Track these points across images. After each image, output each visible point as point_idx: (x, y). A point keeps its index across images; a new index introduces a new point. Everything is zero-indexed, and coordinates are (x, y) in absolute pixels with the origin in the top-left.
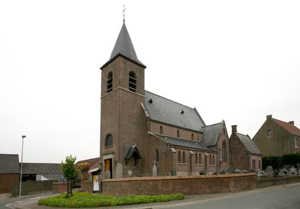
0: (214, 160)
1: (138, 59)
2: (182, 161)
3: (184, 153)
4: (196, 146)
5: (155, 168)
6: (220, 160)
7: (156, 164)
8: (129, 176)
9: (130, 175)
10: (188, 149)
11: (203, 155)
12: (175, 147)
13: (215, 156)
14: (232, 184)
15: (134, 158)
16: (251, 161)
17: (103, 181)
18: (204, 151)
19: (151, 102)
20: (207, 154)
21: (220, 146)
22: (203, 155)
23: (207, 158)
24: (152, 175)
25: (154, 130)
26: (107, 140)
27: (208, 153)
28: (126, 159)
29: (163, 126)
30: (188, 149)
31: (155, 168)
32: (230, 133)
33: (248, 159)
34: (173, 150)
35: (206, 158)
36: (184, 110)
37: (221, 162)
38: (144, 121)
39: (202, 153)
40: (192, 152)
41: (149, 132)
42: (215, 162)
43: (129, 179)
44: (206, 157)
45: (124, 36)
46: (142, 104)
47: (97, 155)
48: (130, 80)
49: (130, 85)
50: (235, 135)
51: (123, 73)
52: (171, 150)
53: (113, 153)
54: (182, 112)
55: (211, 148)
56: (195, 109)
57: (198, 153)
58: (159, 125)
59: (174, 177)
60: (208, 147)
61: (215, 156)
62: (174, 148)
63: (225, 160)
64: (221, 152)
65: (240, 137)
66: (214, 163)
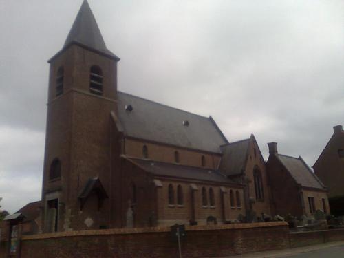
0: (238, 199)
1: (107, 48)
2: (209, 203)
3: (211, 189)
4: (209, 177)
5: (130, 213)
6: (251, 198)
7: (132, 207)
8: (87, 229)
9: (88, 225)
10: (187, 181)
11: (216, 190)
12: (163, 178)
13: (241, 192)
14: (240, 239)
15: (97, 197)
16: (306, 200)
17: (23, 239)
18: (218, 184)
19: (130, 108)
20: (223, 189)
21: (249, 175)
22: (216, 190)
23: (225, 195)
24: (123, 225)
25: (130, 153)
26: (53, 170)
27: (226, 186)
28: (80, 199)
29: (147, 144)
30: (187, 181)
31: (130, 213)
32: (266, 157)
33: (299, 198)
34: (158, 183)
36: (189, 120)
37: (251, 202)
38: (114, 138)
39: (239, 190)
40: (194, 187)
41: (123, 156)
42: (242, 202)
43: (83, 233)
44: (222, 194)
45: (85, 23)
46: (113, 114)
47: (37, 197)
48: (92, 78)
49: (92, 85)
50: (275, 157)
51: (83, 69)
52: (154, 184)
53: (60, 190)
54: (187, 124)
55: (235, 179)
56: (211, 118)
57: (208, 188)
58: (142, 145)
59: (58, 234)
60: (230, 177)
61: (241, 192)
62: (196, 183)
63: (259, 196)
64: (252, 186)
65: (282, 160)
66: (239, 205)
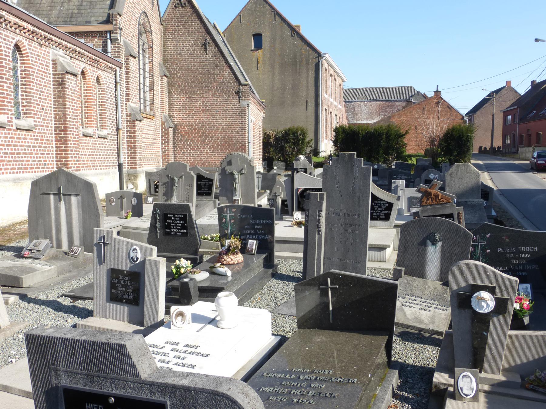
23: (71, 83)
35: (60, 84)
42: (110, 114)
61: (107, 78)
